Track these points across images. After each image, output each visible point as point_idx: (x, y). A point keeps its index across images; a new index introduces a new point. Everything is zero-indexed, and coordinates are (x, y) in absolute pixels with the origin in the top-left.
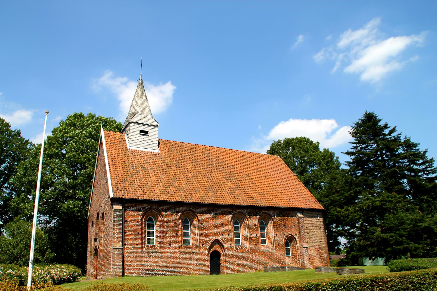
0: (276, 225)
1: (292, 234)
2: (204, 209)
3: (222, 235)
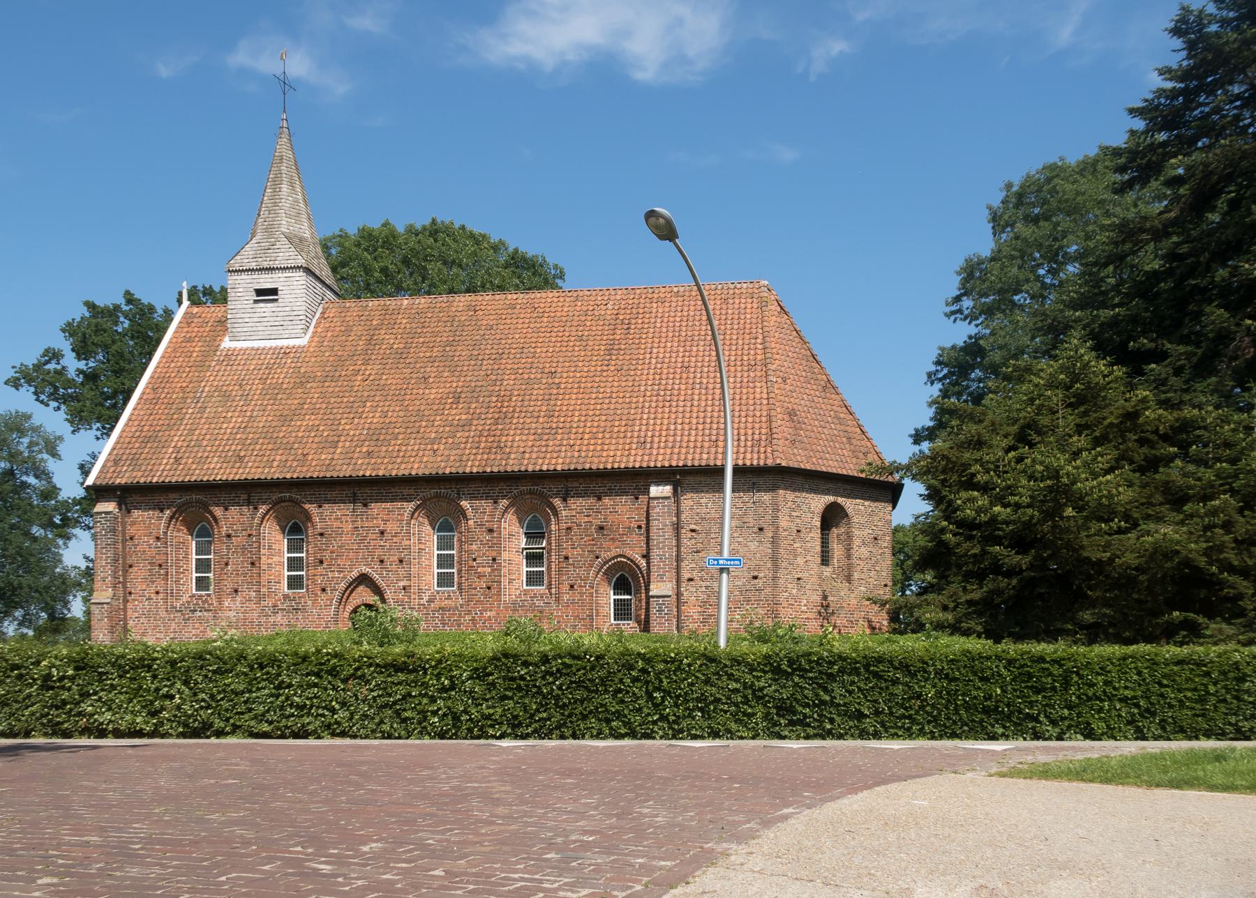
0: (569, 528)
1: (629, 553)
2: (761, 480)
3: (382, 561)
